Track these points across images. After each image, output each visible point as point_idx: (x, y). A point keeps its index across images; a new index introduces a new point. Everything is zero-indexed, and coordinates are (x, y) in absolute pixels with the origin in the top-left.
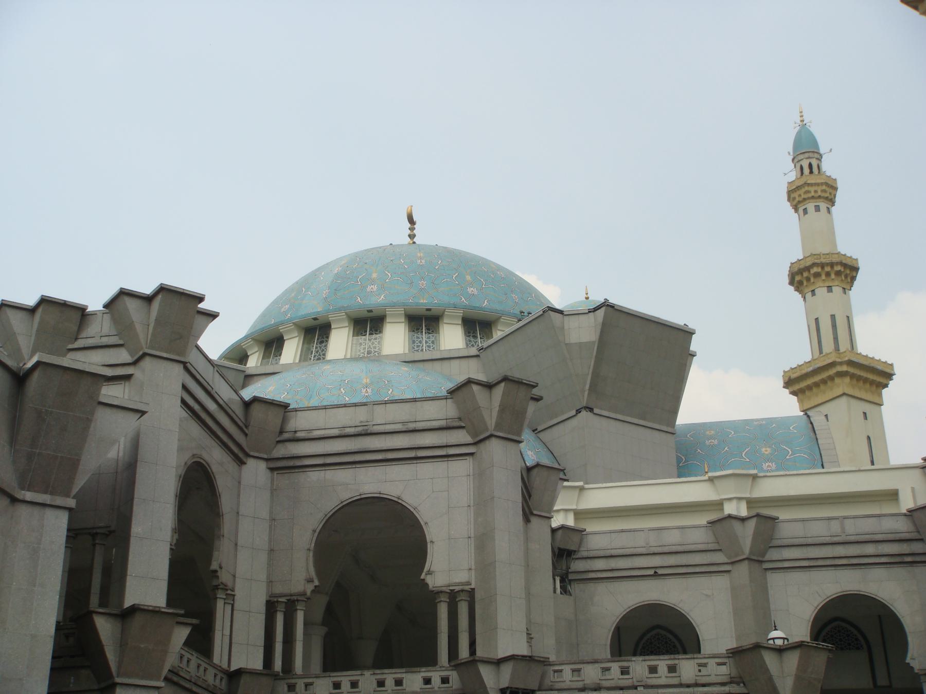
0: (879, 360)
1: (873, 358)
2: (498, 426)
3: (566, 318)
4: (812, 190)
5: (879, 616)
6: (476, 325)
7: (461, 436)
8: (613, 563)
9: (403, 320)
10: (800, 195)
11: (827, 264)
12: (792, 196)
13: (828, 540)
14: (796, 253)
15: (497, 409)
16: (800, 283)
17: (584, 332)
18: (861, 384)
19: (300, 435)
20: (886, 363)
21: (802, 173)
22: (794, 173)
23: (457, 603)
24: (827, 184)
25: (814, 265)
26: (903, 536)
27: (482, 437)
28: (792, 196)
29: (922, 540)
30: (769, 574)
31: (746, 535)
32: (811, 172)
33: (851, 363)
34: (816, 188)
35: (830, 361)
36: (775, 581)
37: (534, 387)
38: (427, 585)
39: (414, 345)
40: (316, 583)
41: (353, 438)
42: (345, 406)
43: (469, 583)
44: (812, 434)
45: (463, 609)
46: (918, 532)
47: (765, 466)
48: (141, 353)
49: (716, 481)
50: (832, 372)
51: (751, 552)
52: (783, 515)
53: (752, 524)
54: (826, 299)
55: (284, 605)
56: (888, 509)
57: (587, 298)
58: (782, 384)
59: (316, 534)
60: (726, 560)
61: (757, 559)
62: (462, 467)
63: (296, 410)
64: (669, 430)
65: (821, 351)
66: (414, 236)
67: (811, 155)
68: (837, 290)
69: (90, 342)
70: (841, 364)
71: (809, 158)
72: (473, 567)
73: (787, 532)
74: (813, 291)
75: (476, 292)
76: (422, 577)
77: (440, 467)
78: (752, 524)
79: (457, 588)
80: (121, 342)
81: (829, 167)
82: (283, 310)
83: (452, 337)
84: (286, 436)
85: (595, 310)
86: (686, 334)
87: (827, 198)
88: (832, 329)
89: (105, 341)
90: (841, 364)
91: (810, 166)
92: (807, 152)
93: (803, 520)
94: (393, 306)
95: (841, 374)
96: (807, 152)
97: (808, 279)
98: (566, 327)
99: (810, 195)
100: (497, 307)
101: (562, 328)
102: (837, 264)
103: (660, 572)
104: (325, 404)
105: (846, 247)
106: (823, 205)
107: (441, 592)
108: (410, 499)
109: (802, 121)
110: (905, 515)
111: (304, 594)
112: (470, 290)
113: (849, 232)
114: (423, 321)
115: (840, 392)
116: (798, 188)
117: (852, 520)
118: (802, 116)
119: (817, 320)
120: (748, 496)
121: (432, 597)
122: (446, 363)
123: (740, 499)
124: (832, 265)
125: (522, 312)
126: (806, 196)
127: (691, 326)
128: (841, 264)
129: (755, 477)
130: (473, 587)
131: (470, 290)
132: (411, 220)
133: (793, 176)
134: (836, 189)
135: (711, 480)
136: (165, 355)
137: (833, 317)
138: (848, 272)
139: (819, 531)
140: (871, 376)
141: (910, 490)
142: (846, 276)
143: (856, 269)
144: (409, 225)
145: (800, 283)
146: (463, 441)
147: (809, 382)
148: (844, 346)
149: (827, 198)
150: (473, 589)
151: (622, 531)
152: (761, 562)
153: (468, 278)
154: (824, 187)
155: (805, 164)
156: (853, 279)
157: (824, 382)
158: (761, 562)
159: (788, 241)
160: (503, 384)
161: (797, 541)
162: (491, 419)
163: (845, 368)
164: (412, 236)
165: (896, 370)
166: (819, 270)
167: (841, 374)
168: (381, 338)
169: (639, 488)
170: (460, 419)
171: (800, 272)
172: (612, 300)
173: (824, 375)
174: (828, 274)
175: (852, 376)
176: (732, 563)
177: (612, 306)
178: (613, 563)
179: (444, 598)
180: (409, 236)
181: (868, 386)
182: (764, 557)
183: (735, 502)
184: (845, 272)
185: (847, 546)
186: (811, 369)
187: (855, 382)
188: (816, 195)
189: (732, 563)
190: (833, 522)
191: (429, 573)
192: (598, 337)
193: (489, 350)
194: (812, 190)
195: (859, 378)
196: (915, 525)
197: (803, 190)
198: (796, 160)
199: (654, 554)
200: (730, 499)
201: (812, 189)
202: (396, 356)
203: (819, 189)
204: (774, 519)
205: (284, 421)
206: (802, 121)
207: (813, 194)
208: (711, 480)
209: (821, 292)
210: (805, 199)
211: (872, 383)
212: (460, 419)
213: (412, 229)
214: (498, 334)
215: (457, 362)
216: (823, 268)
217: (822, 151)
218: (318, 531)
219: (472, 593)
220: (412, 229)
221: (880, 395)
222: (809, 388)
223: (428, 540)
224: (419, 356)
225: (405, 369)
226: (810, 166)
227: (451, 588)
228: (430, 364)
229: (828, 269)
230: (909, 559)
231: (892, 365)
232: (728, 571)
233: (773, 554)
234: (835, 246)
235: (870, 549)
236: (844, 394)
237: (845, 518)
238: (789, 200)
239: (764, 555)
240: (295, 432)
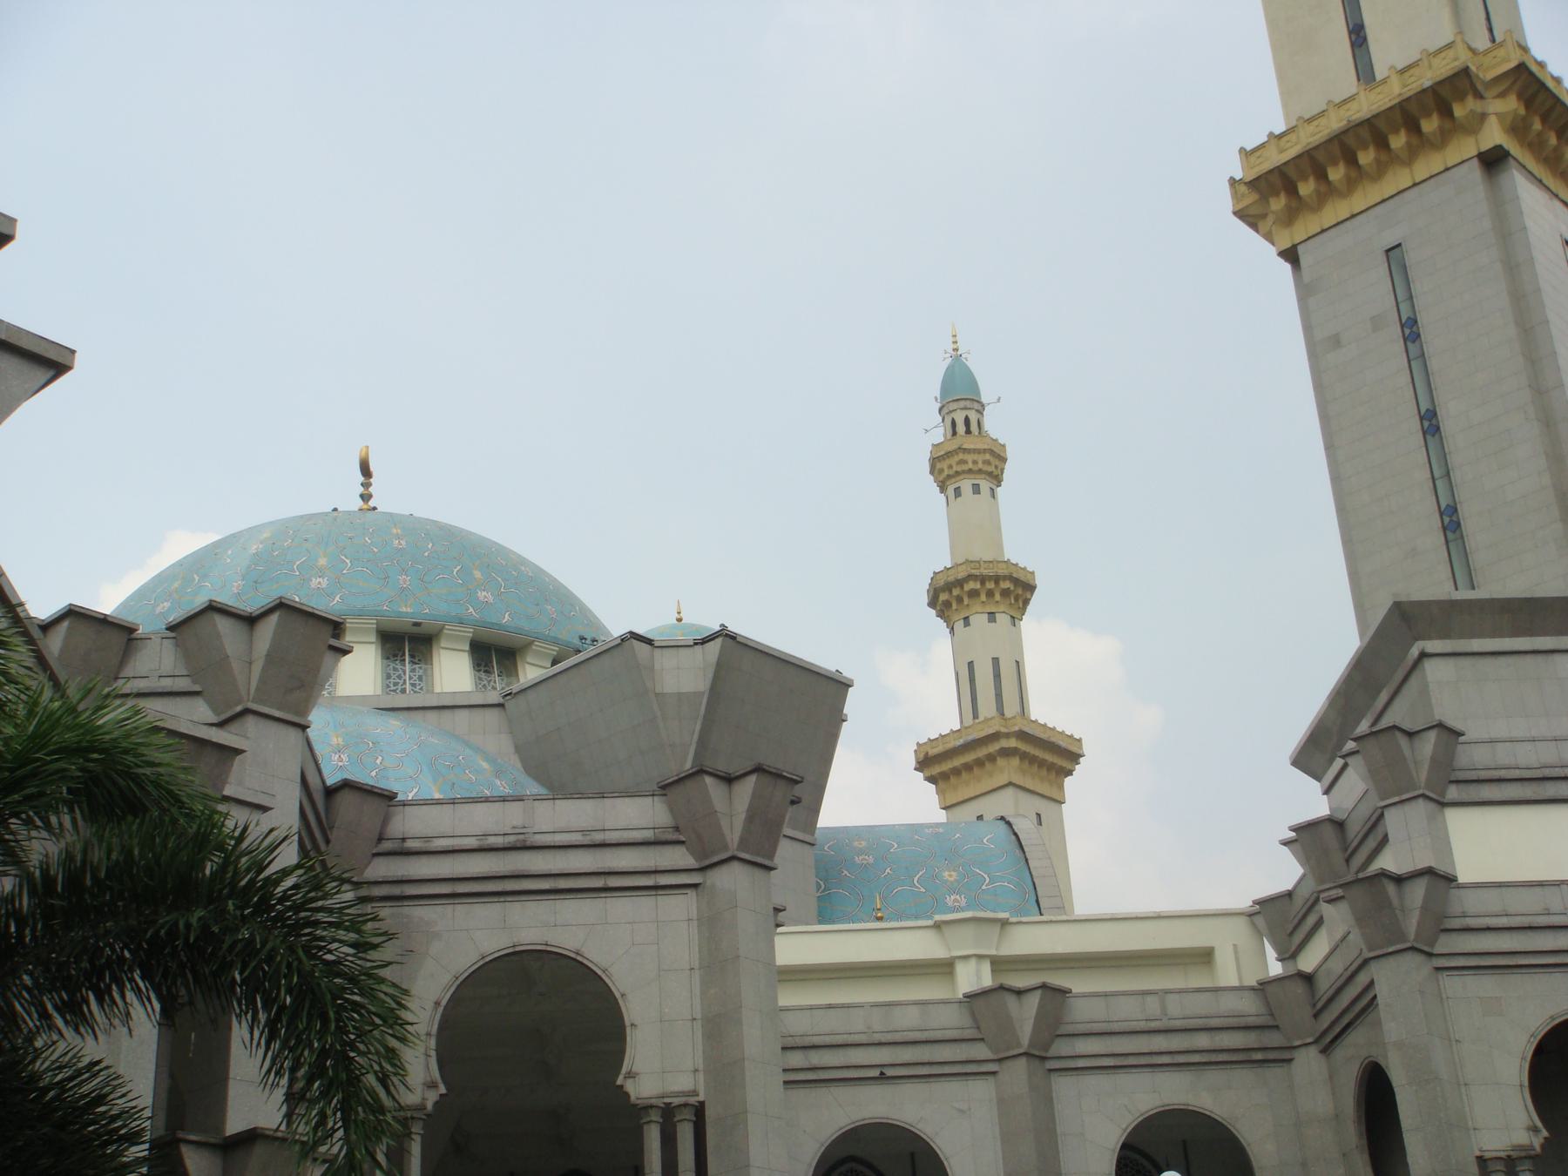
0: (1062, 733)
1: (1053, 729)
2: (743, 843)
3: (657, 652)
4: (967, 460)
5: (1184, 1142)
6: (493, 654)
7: (678, 857)
8: (816, 1058)
9: (373, 639)
10: (950, 467)
11: (990, 578)
12: (939, 466)
13: (1142, 1025)
14: (941, 559)
15: (743, 816)
16: (947, 604)
17: (686, 677)
18: (1044, 772)
19: (410, 844)
20: (1071, 737)
21: (954, 433)
22: (941, 430)
23: (675, 1126)
24: (992, 452)
25: (970, 577)
26: (1251, 1021)
27: (716, 859)
28: (939, 466)
29: (1277, 1027)
30: (1055, 1078)
31: (1025, 1015)
32: (968, 432)
33: (1022, 735)
34: (975, 457)
35: (991, 731)
36: (1064, 1087)
37: (796, 782)
38: (627, 1095)
39: (390, 682)
40: (443, 1090)
41: (501, 854)
42: (487, 800)
43: (695, 1093)
44: (1018, 851)
45: (685, 1134)
46: (1272, 1015)
47: (950, 900)
48: (239, 708)
49: (944, 928)
50: (993, 748)
51: (1031, 1044)
52: (1078, 984)
53: (1034, 1001)
54: (983, 631)
55: (421, 1124)
56: (1197, 979)
57: (679, 620)
58: (913, 763)
59: (441, 1009)
60: (991, 1056)
61: (1037, 1055)
62: (679, 907)
63: (404, 804)
64: (808, 838)
65: (975, 716)
66: (370, 496)
67: (968, 404)
68: (1003, 619)
69: (141, 685)
70: (1007, 735)
71: (965, 408)
72: (701, 1067)
73: (1082, 1013)
74: (966, 619)
75: (491, 599)
76: (619, 1082)
77: (645, 903)
78: (1034, 1001)
79: (676, 1101)
80: (197, 688)
81: (995, 424)
82: (159, 609)
83: (453, 672)
84: (387, 846)
85: (704, 641)
86: (838, 686)
87: (990, 474)
88: (991, 680)
89: (167, 684)
90: (1007, 735)
91: (967, 421)
92: (961, 399)
93: (1106, 995)
94: (360, 614)
95: (1007, 753)
96: (961, 399)
97: (960, 600)
98: (657, 666)
99: (965, 467)
100: (525, 625)
101: (652, 669)
102: (1005, 578)
103: (889, 1072)
105: (1018, 551)
106: (985, 485)
107: (652, 1107)
108: (597, 955)
109: (956, 350)
110: (1252, 989)
111: (421, 1107)
112: (482, 595)
113: (1023, 531)
114: (407, 643)
115: (1003, 780)
116: (949, 454)
117: (1176, 996)
119: (971, 664)
120: (993, 952)
121: (637, 1113)
122: (447, 714)
123: (980, 957)
124: (997, 579)
125: (582, 638)
127: (847, 673)
128: (1011, 578)
129: (1004, 923)
130: (701, 1098)
131: (482, 595)
132: (366, 470)
133: (938, 435)
134: (1004, 460)
135: (938, 926)
136: (277, 714)
137: (996, 661)
138: (1020, 591)
139: (1128, 1012)
140: (1049, 757)
141: (1231, 949)
142: (1016, 599)
143: (1030, 588)
144: (362, 479)
145: (947, 604)
146: (682, 864)
147: (958, 762)
148: (1011, 709)
149: (990, 474)
150: (702, 1104)
151: (830, 1007)
152: (1043, 1059)
153: (477, 574)
154: (987, 457)
155: (960, 418)
156: (1026, 602)
157: (980, 763)
158: (1043, 1059)
159: (927, 539)
160: (753, 778)
161: (1097, 1027)
162: (733, 828)
163: (1012, 743)
164: (366, 497)
165: (1086, 749)
166: (978, 586)
167: (1007, 753)
169: (805, 937)
170: (677, 829)
171: (948, 587)
172: (733, 627)
173: (981, 753)
174: (990, 594)
175: (1024, 756)
176: (1000, 1060)
177: (732, 637)
178: (816, 1058)
179: (655, 1116)
180: (362, 496)
181: (1035, 768)
182: (1047, 1050)
183: (973, 962)
184: (1011, 590)
185: (1170, 1036)
186: (961, 741)
187: (1026, 765)
188: (975, 468)
189: (1000, 1060)
190: (1149, 999)
191: (631, 1075)
192: (708, 686)
193: (521, 697)
194: (967, 460)
195: (1033, 760)
196: (1268, 1004)
197: (956, 458)
198: (945, 410)
199: (880, 1044)
200: (966, 958)
201: (969, 458)
202: (363, 699)
203: (980, 458)
204: (1064, 992)
205: (386, 821)
206: (956, 350)
207: (970, 465)
208: (938, 926)
209: (978, 620)
210: (957, 473)
211: (1051, 767)
212: (677, 829)
213: (366, 485)
214: (530, 672)
215: (464, 713)
217: (984, 400)
218: (444, 1003)
219: (700, 1111)
220: (366, 485)
221: (1061, 787)
222: (956, 772)
223: (627, 1023)
224: (401, 701)
225: (394, 723)
226: (967, 421)
227: (667, 1100)
228: (419, 714)
229: (990, 585)
230: (1259, 1056)
231: (1079, 740)
232: (994, 1073)
233: (1062, 1047)
234: (1000, 547)
235: (1203, 1041)
236: (1010, 784)
237: (1167, 992)
238: (932, 472)
239: (1047, 1047)
240: (404, 839)
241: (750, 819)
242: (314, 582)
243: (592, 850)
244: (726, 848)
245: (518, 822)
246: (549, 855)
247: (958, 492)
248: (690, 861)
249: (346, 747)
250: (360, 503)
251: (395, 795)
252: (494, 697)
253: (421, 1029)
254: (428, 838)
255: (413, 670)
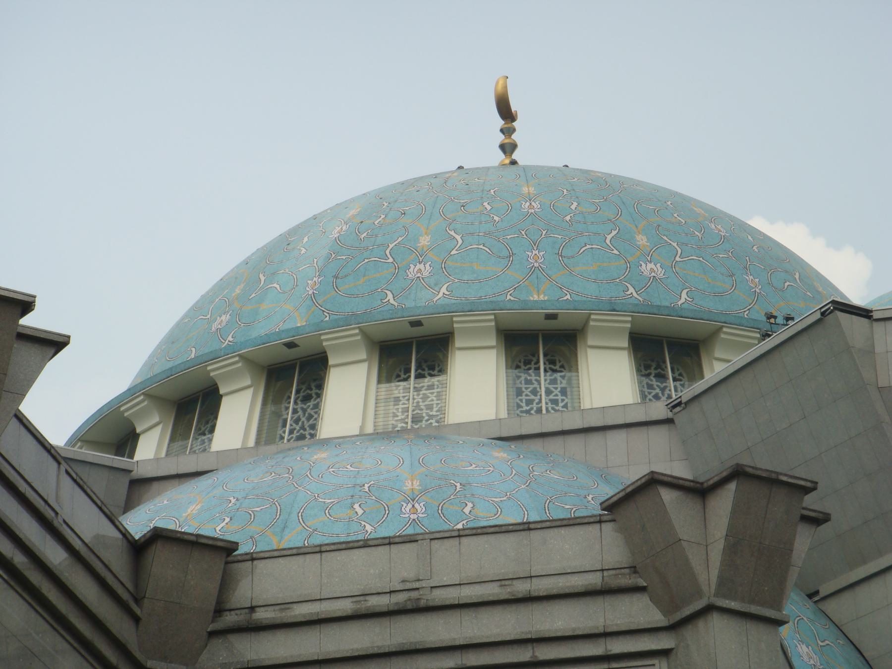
2: (725, 585)
3: (878, 327)
6: (664, 349)
9: (493, 342)
19: (262, 615)
37: (807, 490)
42: (365, 544)
63: (252, 558)
66: (514, 146)
75: (660, 273)
82: (215, 326)
84: (230, 619)
94: (471, 309)
98: (879, 349)
101: (870, 351)
112: (647, 268)
114: (540, 344)
122: (595, 439)
125: (770, 316)
131: (647, 268)
132: (505, 111)
144: (500, 122)
153: (642, 240)
160: (732, 486)
162: (707, 566)
164: (508, 148)
170: (634, 569)
180: (502, 147)
193: (695, 408)
205: (226, 583)
212: (634, 569)
213: (507, 131)
215: (621, 435)
220: (507, 131)
225: (501, 454)
240: (252, 609)
241: (733, 546)
242: (412, 272)
243: (513, 608)
244: (698, 593)
245: (409, 573)
246: (453, 618)
248: (656, 617)
249: (425, 491)
250: (501, 156)
251: (234, 546)
252: (659, 410)
254: (285, 605)
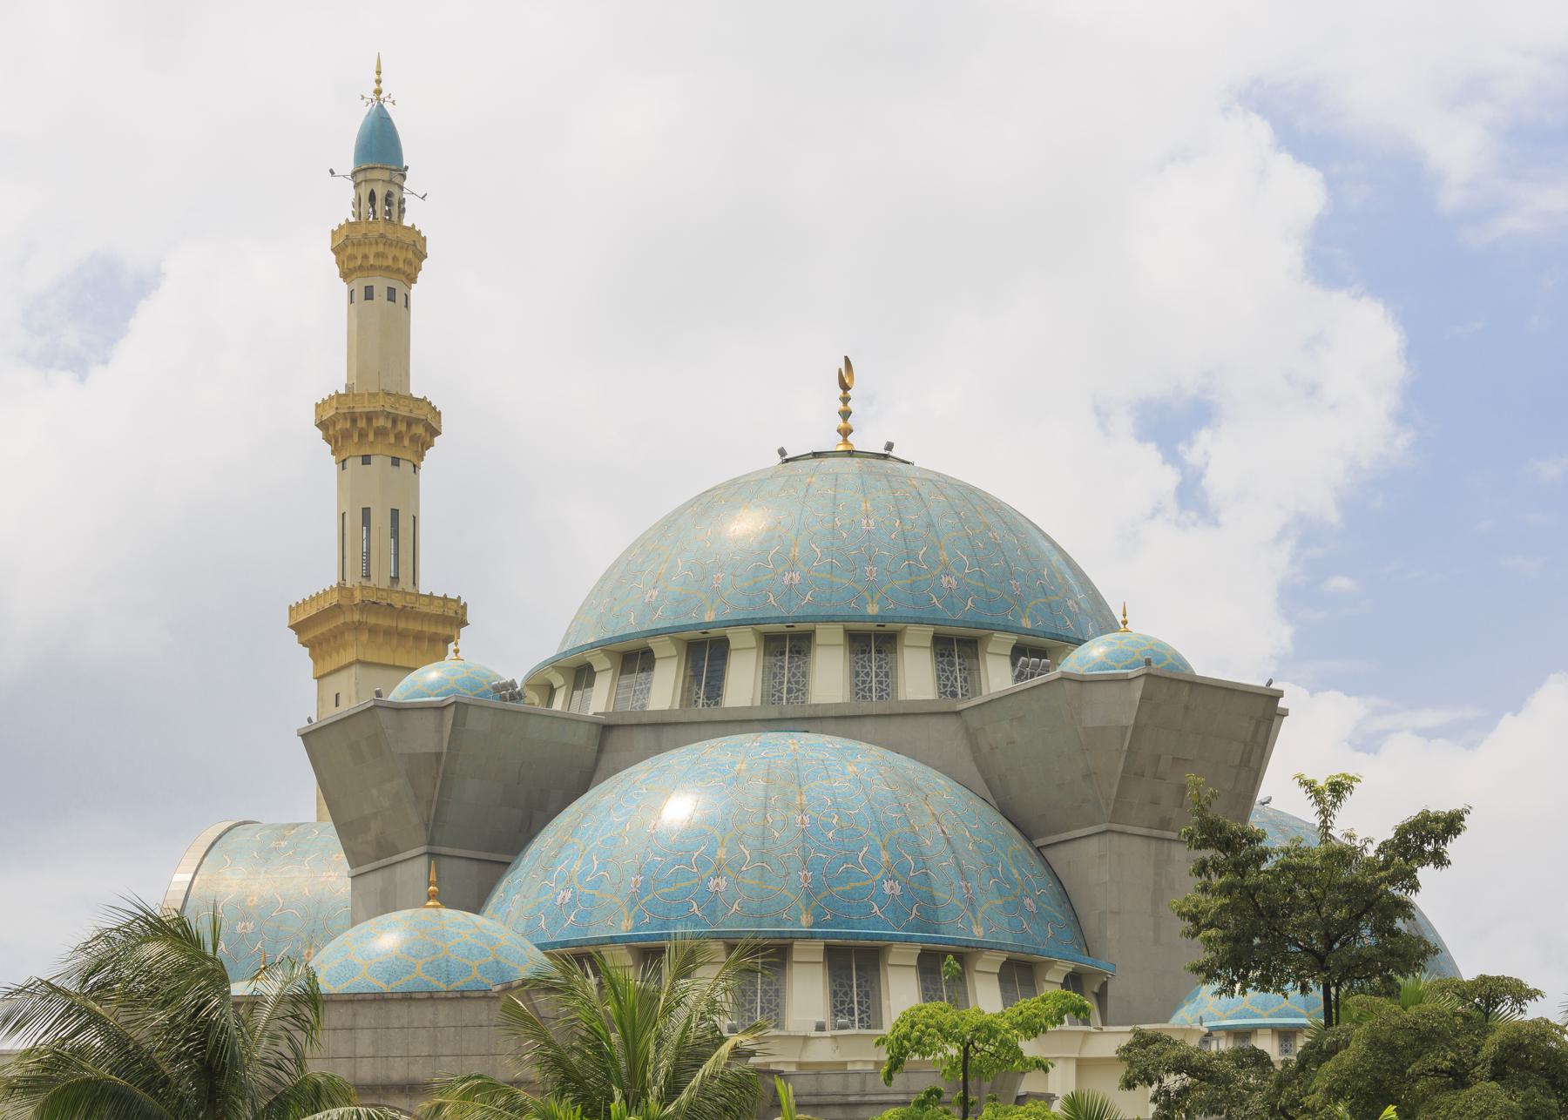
4: (380, 255)
9: (928, 643)
68: (380, 462)
71: (390, 181)
95: (357, 627)
104: (459, 984)
118: (379, 82)
124: (410, 422)
126: (379, 262)
166: (389, 425)
167: (357, 627)
168: (648, 682)
174: (399, 437)
175: (373, 630)
194: (380, 255)
201: (391, 252)
206: (378, 92)
207: (390, 262)
213: (845, 400)
216: (395, 422)
220: (845, 400)
226: (389, 195)
247: (369, 293)
253: (260, 986)
255: (880, 667)
